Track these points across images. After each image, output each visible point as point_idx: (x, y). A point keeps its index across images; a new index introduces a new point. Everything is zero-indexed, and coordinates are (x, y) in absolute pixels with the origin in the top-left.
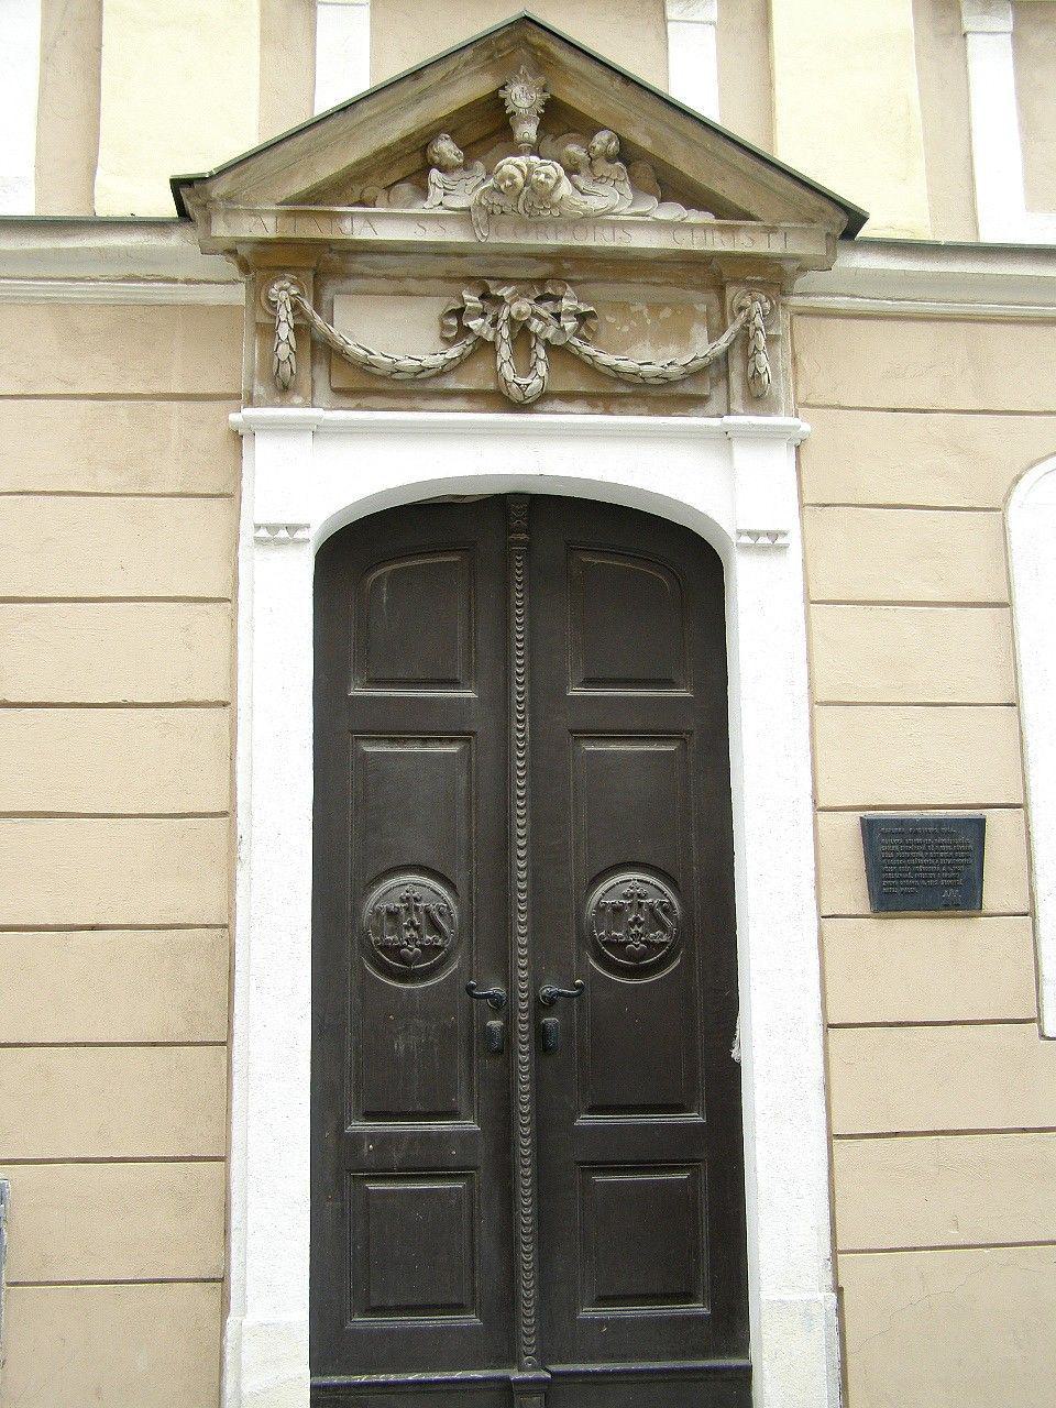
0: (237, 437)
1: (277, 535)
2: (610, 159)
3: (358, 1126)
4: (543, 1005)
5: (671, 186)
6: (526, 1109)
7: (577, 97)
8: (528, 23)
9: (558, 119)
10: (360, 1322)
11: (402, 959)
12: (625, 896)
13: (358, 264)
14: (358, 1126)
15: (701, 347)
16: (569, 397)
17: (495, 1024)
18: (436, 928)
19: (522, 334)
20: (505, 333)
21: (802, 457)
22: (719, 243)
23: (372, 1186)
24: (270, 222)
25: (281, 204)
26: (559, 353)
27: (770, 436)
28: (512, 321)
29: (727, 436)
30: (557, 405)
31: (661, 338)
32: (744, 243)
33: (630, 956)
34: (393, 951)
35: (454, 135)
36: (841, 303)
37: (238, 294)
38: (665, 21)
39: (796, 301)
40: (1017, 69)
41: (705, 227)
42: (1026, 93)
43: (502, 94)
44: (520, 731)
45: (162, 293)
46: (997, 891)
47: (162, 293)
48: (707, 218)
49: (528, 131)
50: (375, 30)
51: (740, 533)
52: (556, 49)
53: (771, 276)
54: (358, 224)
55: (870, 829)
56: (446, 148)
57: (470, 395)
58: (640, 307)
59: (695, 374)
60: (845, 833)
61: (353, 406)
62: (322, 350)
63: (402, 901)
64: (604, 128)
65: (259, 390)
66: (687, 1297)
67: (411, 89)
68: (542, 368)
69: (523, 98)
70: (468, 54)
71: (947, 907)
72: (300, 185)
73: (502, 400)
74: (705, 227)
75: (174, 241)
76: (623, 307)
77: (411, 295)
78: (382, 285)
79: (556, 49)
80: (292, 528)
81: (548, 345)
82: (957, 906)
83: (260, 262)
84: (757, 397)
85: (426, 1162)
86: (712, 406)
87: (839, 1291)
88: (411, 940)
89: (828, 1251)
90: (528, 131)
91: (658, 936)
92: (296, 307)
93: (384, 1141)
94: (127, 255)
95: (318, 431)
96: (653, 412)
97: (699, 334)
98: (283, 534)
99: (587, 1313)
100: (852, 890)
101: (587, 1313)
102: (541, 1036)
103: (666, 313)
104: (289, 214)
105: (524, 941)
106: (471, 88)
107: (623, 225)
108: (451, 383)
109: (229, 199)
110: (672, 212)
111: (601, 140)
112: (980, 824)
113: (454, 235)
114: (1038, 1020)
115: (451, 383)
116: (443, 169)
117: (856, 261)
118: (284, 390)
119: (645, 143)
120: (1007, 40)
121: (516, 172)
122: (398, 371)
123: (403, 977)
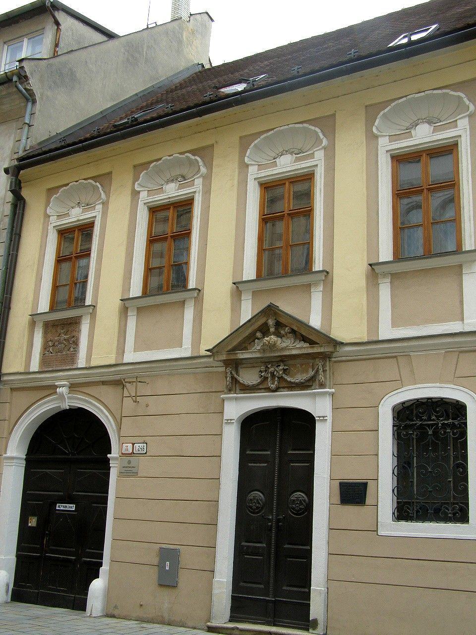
0: (223, 400)
1: (229, 422)
2: (290, 333)
3: (243, 544)
4: (278, 521)
6: (273, 542)
7: (282, 320)
9: (278, 325)
10: (242, 584)
11: (296, 510)
12: (296, 498)
13: (244, 362)
14: (243, 544)
15: (311, 373)
16: (284, 388)
18: (259, 503)
19: (273, 375)
20: (269, 375)
22: (310, 351)
23: (246, 556)
25: (227, 352)
28: (271, 373)
29: (315, 395)
30: (282, 390)
31: (303, 372)
32: (316, 350)
33: (296, 510)
34: (251, 507)
35: (261, 331)
36: (344, 358)
37: (223, 369)
39: (333, 359)
41: (307, 347)
42: (393, 296)
44: (277, 461)
46: (369, 500)
48: (307, 345)
49: (272, 330)
50: (253, 304)
54: (240, 355)
55: (340, 483)
56: (259, 335)
57: (265, 389)
58: (299, 365)
59: (309, 380)
60: (336, 484)
62: (235, 381)
63: (296, 498)
64: (287, 326)
65: (226, 391)
67: (248, 325)
68: (276, 383)
69: (271, 322)
70: (260, 314)
71: (357, 503)
72: (230, 347)
73: (268, 390)
75: (212, 359)
76: (294, 365)
77: (255, 367)
78: (249, 365)
80: (231, 420)
81: (278, 378)
82: (359, 503)
83: (227, 363)
84: (322, 386)
85: (255, 551)
86: (313, 387)
87: (328, 589)
88: (297, 506)
90: (272, 330)
91: (302, 507)
92: (231, 373)
93: (248, 547)
94: (204, 363)
95: (236, 399)
96: (301, 390)
97: (310, 370)
98: (229, 421)
99: (285, 588)
100: (337, 499)
101: (285, 588)
102: (278, 527)
103: (304, 366)
104: (228, 354)
105: (275, 507)
106: (262, 321)
108: (261, 387)
109: (217, 352)
110: (303, 344)
112: (365, 485)
113: (258, 355)
115: (261, 387)
116: (258, 339)
118: (230, 391)
120: (389, 284)
121: (266, 341)
123: (254, 513)
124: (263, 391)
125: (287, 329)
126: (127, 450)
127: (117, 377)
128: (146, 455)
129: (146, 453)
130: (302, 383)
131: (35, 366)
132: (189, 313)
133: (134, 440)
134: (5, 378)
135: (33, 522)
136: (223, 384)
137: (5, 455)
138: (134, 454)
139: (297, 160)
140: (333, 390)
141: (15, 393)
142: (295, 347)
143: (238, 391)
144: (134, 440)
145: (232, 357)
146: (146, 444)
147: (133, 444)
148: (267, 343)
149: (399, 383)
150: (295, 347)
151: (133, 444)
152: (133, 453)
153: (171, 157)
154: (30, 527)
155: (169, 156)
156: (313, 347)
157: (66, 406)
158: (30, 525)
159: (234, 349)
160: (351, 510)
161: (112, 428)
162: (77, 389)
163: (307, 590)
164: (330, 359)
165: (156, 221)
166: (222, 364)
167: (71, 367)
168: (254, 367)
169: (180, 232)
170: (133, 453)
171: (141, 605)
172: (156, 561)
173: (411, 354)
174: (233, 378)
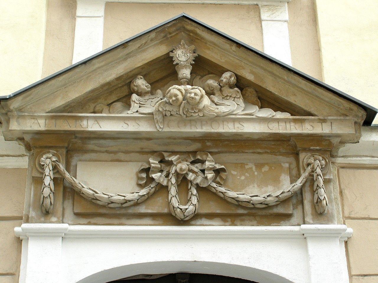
0: (19, 241)
8: (185, 19)
13: (91, 145)
16: (211, 216)
20: (173, 181)
21: (349, 248)
22: (294, 129)
28: (177, 174)
30: (204, 221)
31: (263, 182)
36: (366, 161)
41: (285, 120)
43: (171, 55)
49: (186, 73)
54: (91, 122)
56: (141, 83)
59: (284, 201)
67: (122, 53)
68: (194, 200)
70: (153, 35)
72: (59, 102)
76: (241, 166)
86: (294, 220)
90: (186, 73)
95: (65, 237)
96: (260, 224)
103: (266, 169)
104: (53, 117)
109: (20, 110)
113: (144, 127)
115: (143, 209)
116: (139, 94)
122: (112, 203)
125: (227, 75)
130: (268, 206)
140: (350, 230)
143: (69, 213)
148: (180, 97)
156: (302, 121)
161: (278, 120)
164: (333, 159)
166: (19, 148)
174: (58, 181)
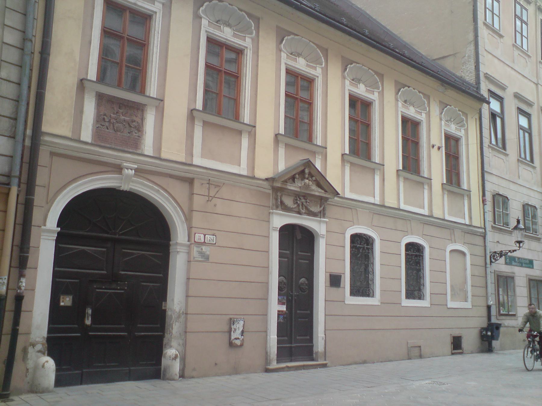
1: (274, 229)
5: (319, 185)
7: (313, 172)
9: (310, 174)
17: (290, 298)
24: (280, 184)
26: (306, 208)
27: (324, 222)
38: (316, 157)
40: (350, 172)
41: (323, 193)
45: (262, 189)
47: (262, 189)
48: (323, 191)
49: (307, 176)
51: (321, 235)
52: (311, 165)
53: (327, 199)
56: (297, 176)
57: (295, 211)
60: (328, 275)
61: (372, 265)
62: (282, 203)
66: (307, 336)
69: (307, 171)
74: (323, 193)
79: (311, 165)
89: (324, 330)
100: (328, 284)
103: (315, 203)
104: (282, 183)
106: (301, 168)
107: (315, 191)
108: (294, 210)
110: (320, 190)
111: (314, 178)
112: (341, 276)
113: (298, 190)
114: (344, 301)
117: (336, 198)
118: (277, 208)
119: (318, 179)
124: (294, 212)
126: (200, 239)
127: (118, 162)
128: (215, 245)
129: (215, 244)
131: (87, 135)
132: (245, 142)
133: (205, 232)
134: (47, 138)
135: (66, 301)
136: (271, 202)
137: (43, 227)
138: (205, 243)
139: (308, 66)
141: (54, 158)
142: (317, 192)
144: (205, 232)
145: (284, 187)
146: (216, 236)
147: (205, 235)
149: (353, 223)
150: (317, 192)
151: (205, 235)
152: (204, 242)
153: (231, 6)
154: (63, 307)
155: (229, 4)
157: (125, 187)
158: (62, 304)
159: (285, 182)
160: (334, 289)
162: (142, 175)
163: (278, 346)
165: (297, 96)
167: (135, 151)
168: (289, 195)
169: (231, 72)
170: (204, 242)
171: (216, 364)
172: (525, 276)
173: (358, 209)
